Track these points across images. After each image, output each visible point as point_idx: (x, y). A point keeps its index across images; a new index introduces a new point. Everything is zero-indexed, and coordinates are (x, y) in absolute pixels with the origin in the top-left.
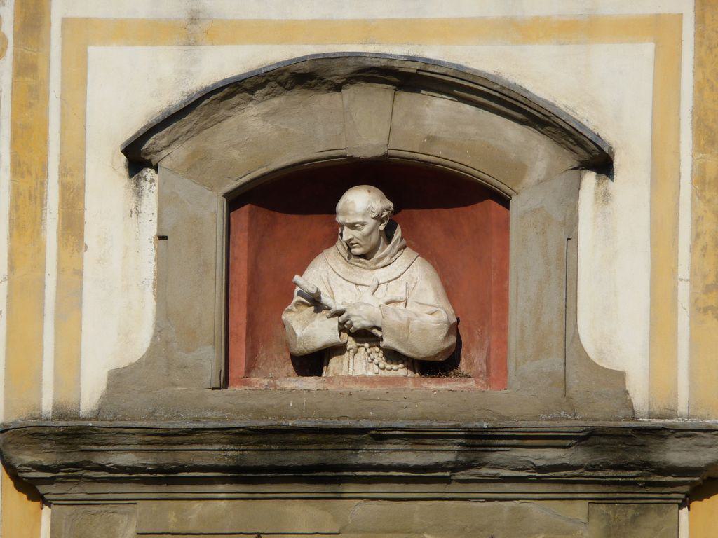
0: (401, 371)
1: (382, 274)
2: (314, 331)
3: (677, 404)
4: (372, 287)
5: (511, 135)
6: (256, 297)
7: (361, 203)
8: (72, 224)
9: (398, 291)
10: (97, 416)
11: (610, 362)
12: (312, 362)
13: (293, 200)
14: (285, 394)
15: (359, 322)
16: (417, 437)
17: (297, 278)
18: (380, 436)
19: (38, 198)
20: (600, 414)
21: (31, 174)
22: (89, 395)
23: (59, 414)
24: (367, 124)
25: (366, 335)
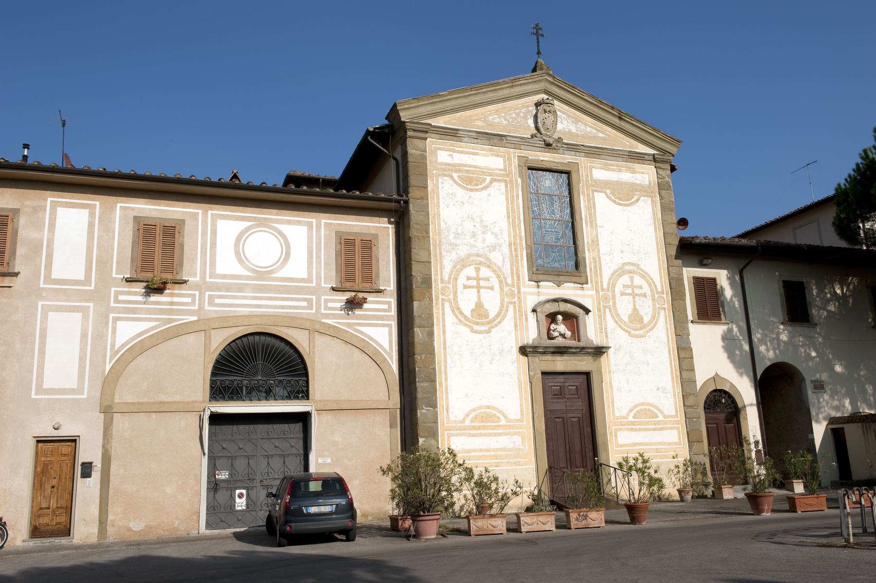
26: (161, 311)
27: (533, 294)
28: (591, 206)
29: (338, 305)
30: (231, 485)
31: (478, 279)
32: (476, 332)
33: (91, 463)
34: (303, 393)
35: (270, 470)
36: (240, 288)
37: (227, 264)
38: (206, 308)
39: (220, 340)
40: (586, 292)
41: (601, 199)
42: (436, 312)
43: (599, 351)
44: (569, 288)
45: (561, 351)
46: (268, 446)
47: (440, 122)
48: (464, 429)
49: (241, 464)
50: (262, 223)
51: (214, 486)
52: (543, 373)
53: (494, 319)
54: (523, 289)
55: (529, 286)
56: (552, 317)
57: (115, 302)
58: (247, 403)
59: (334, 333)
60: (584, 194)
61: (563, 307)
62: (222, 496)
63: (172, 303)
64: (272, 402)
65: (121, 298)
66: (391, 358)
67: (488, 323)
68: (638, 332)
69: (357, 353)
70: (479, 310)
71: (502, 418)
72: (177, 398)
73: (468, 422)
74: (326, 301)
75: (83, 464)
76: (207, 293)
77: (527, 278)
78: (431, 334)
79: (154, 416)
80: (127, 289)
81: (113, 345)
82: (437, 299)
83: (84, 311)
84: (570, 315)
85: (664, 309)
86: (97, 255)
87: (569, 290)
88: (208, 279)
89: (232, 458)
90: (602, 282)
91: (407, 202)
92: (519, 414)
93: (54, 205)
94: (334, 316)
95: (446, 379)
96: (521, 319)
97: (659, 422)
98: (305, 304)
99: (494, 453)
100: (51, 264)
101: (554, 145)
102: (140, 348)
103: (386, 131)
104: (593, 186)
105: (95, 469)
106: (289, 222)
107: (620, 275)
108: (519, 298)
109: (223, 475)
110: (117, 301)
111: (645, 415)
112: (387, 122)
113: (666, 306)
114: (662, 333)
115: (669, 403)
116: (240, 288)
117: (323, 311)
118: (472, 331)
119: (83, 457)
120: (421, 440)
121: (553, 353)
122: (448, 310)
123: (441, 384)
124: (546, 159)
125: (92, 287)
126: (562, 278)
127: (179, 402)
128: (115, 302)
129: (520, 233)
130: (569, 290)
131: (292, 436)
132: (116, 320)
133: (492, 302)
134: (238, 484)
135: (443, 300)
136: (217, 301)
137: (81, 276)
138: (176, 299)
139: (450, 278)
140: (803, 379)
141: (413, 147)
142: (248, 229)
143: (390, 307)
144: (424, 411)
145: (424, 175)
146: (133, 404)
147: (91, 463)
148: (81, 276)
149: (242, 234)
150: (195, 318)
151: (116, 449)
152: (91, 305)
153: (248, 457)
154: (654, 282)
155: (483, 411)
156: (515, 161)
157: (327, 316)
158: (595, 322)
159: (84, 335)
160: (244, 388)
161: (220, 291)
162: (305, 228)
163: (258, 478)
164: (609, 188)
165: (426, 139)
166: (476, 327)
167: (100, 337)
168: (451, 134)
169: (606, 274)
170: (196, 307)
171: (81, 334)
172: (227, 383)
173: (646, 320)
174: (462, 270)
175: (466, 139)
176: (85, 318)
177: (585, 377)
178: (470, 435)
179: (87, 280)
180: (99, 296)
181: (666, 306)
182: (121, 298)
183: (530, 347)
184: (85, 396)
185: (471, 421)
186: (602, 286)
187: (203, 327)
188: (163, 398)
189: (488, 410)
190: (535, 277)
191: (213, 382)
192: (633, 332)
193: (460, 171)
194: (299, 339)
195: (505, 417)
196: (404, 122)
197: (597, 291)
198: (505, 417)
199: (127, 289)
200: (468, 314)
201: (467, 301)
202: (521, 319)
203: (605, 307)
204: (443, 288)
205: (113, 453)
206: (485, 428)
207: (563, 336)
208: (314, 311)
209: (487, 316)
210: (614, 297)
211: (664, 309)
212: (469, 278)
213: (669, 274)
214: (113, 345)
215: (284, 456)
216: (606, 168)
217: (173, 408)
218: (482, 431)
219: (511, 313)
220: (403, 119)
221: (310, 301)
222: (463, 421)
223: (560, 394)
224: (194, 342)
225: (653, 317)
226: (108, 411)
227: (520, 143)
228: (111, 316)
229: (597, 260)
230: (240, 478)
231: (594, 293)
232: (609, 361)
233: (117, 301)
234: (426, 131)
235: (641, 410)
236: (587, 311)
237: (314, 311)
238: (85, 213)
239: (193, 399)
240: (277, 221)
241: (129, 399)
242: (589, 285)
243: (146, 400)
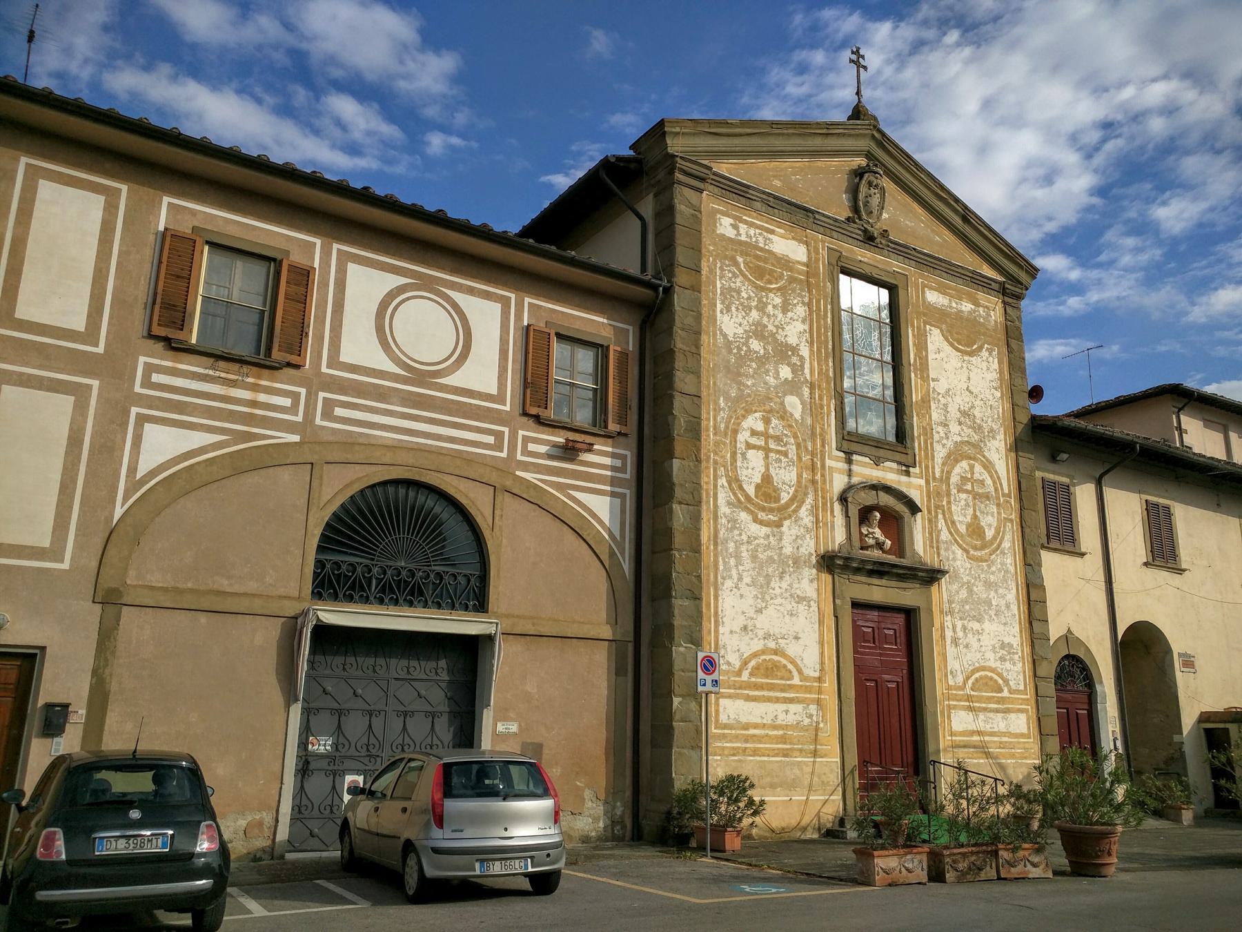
26: (232, 416)
27: (840, 471)
28: (922, 346)
29: (543, 449)
30: (335, 765)
31: (766, 436)
32: (761, 523)
33: (66, 706)
34: (480, 604)
35: (407, 740)
36: (381, 395)
37: (359, 347)
38: (318, 421)
39: (337, 488)
40: (913, 480)
41: (935, 339)
42: (706, 480)
43: (931, 576)
44: (891, 470)
45: (879, 571)
46: (406, 693)
47: (724, 168)
48: (740, 688)
49: (355, 727)
50: (428, 285)
51: (305, 768)
52: (856, 605)
53: (787, 505)
54: (829, 463)
55: (837, 459)
56: (865, 515)
57: (143, 386)
58: (432, 613)
59: (536, 501)
60: (913, 326)
61: (886, 499)
62: (318, 784)
63: (254, 404)
64: (419, 612)
65: (156, 378)
66: (623, 554)
67: (780, 510)
68: (978, 553)
69: (570, 537)
70: (767, 487)
71: (795, 673)
72: (252, 586)
73: (745, 676)
74: (526, 440)
75: (49, 706)
76: (322, 395)
77: (834, 446)
78: (696, 518)
79: (203, 619)
80: (170, 364)
81: (132, 469)
82: (708, 460)
83: (80, 393)
84: (886, 512)
85: (1011, 521)
86: (115, 288)
87: (889, 474)
88: (324, 369)
89: (340, 713)
90: (933, 468)
91: (668, 291)
92: (818, 667)
93: (33, 175)
94: (537, 469)
95: (716, 598)
96: (825, 510)
97: (1002, 700)
98: (490, 439)
99: (781, 732)
100: (17, 288)
101: (878, 240)
102: (185, 481)
103: (632, 166)
104: (925, 315)
105: (73, 718)
106: (471, 291)
107: (957, 461)
108: (823, 475)
109: (321, 745)
110: (147, 383)
111: (986, 686)
112: (632, 153)
113: (1013, 517)
114: (1008, 559)
115: (1016, 673)
116: (381, 395)
117: (519, 457)
118: (756, 520)
119: (49, 690)
120: (676, 701)
121: (871, 573)
122: (723, 481)
123: (709, 605)
124: (865, 260)
125: (100, 349)
126: (882, 453)
127: (254, 595)
128: (143, 386)
129: (827, 370)
130: (889, 474)
131: (328, 672)
132: (142, 420)
133: (786, 477)
134: (348, 764)
135: (716, 462)
136: (339, 411)
137: (78, 323)
138: (262, 397)
139: (727, 427)
140: (1169, 651)
141: (683, 198)
142: (401, 289)
143: (624, 464)
144: (681, 649)
145: (696, 250)
146: (165, 590)
147: (66, 706)
148: (78, 323)
149: (391, 296)
150: (296, 438)
151: (120, 679)
152: (95, 383)
153: (340, 713)
154: (999, 478)
155: (768, 658)
156: (823, 253)
157: (526, 466)
158: (924, 528)
159: (74, 442)
160: (374, 581)
161: (345, 394)
162: (497, 307)
163: (757, 819)
164: (946, 322)
165: (701, 191)
166: (762, 515)
167: (107, 450)
168: (738, 192)
169: (940, 453)
170: (300, 418)
171: (69, 438)
172: (344, 567)
173: (989, 534)
174: (744, 417)
175: (758, 205)
176: (80, 409)
177: (900, 619)
178: (749, 699)
179: (91, 334)
180: (113, 367)
181: (1013, 517)
182: (156, 378)
183: (841, 557)
184: (65, 566)
185: (751, 674)
186: (934, 473)
187: (312, 455)
188: (224, 584)
189: (774, 657)
190: (845, 445)
191: (320, 564)
192: (972, 552)
193: (747, 254)
194: (477, 500)
195: (800, 672)
196: (674, 156)
197: (927, 482)
198: (800, 672)
199: (170, 364)
200: (751, 491)
201: (752, 468)
202: (825, 510)
203: (937, 507)
204: (717, 444)
205: (114, 687)
206: (772, 687)
207: (880, 545)
208: (504, 455)
209: (778, 499)
210: (949, 494)
211: (1011, 521)
212: (754, 433)
213: (1018, 468)
214: (132, 469)
215: (405, 714)
216: (942, 290)
217: (243, 605)
218: (765, 693)
219: (809, 500)
220: (670, 150)
221: (499, 436)
222: (739, 673)
223: (876, 638)
224: (289, 481)
225: (997, 532)
226: (110, 600)
227: (831, 227)
228: (134, 410)
229: (928, 432)
230: (352, 752)
231: (922, 482)
232: (943, 591)
233: (147, 383)
234: (702, 178)
235: (981, 677)
236: (914, 508)
237: (504, 455)
238: (96, 203)
239: (282, 591)
240: (453, 286)
241: (156, 579)
242: (917, 470)
243: (190, 585)
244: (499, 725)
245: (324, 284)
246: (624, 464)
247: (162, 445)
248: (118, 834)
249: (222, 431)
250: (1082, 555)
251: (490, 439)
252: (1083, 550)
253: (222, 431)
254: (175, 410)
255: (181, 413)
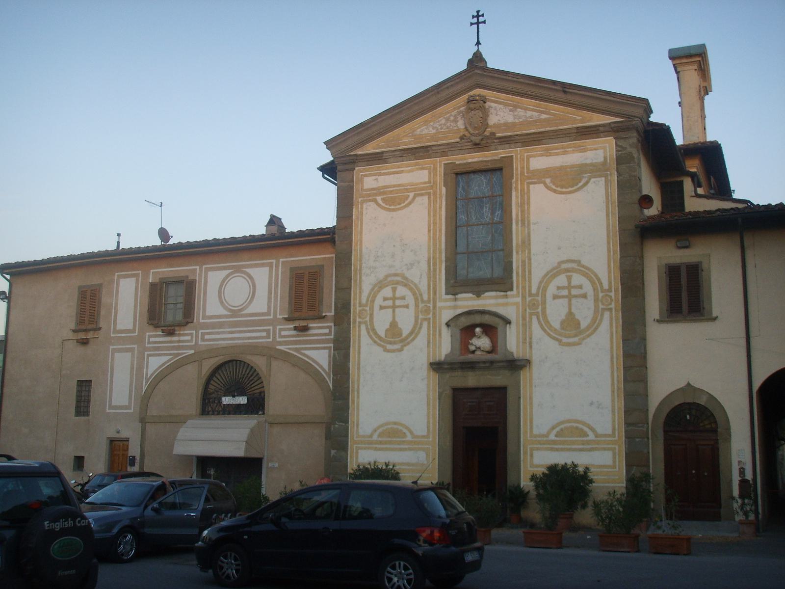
0: (485, 353)
1: (482, 340)
2: (472, 348)
3: (532, 357)
4: (482, 342)
5: (497, 320)
6: (464, 346)
7: (478, 330)
8: (440, 335)
9: (483, 342)
10: (445, 360)
11: (512, 351)
12: (473, 352)
13: (468, 332)
14: (471, 357)
15: (478, 346)
16: (484, 362)
17: (470, 341)
18: (478, 362)
19: (436, 331)
20: (510, 358)
21: (594, 502)
22: (443, 358)
23: (439, 360)
24: (478, 319)
25: (479, 348)
26: (174, 348)
36: (221, 325)
50: (238, 270)
59: (286, 357)
63: (179, 341)
67: (402, 341)
85: (610, 310)
94: (286, 343)
97: (588, 442)
98: (264, 334)
125: (137, 334)
143: (330, 331)
150: (193, 352)
154: (599, 280)
157: (280, 343)
166: (389, 347)
167: (140, 369)
180: (140, 340)
181: (613, 306)
187: (197, 358)
194: (259, 362)
197: (524, 297)
201: (382, 321)
206: (391, 443)
212: (385, 299)
218: (388, 446)
226: (143, 421)
228: (271, 328)
231: (519, 300)
233: (149, 343)
236: (508, 322)
241: (155, 413)
244: (270, 464)
245: (200, 286)
246: (330, 331)
247: (155, 363)
248: (760, 511)
249: (170, 354)
250: (715, 319)
251: (264, 334)
252: (714, 315)
253: (170, 354)
254: (157, 350)
255: (158, 351)
